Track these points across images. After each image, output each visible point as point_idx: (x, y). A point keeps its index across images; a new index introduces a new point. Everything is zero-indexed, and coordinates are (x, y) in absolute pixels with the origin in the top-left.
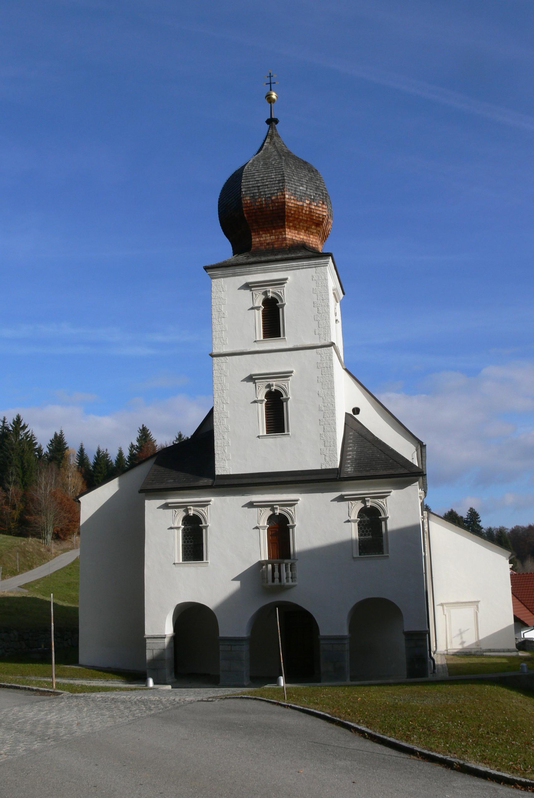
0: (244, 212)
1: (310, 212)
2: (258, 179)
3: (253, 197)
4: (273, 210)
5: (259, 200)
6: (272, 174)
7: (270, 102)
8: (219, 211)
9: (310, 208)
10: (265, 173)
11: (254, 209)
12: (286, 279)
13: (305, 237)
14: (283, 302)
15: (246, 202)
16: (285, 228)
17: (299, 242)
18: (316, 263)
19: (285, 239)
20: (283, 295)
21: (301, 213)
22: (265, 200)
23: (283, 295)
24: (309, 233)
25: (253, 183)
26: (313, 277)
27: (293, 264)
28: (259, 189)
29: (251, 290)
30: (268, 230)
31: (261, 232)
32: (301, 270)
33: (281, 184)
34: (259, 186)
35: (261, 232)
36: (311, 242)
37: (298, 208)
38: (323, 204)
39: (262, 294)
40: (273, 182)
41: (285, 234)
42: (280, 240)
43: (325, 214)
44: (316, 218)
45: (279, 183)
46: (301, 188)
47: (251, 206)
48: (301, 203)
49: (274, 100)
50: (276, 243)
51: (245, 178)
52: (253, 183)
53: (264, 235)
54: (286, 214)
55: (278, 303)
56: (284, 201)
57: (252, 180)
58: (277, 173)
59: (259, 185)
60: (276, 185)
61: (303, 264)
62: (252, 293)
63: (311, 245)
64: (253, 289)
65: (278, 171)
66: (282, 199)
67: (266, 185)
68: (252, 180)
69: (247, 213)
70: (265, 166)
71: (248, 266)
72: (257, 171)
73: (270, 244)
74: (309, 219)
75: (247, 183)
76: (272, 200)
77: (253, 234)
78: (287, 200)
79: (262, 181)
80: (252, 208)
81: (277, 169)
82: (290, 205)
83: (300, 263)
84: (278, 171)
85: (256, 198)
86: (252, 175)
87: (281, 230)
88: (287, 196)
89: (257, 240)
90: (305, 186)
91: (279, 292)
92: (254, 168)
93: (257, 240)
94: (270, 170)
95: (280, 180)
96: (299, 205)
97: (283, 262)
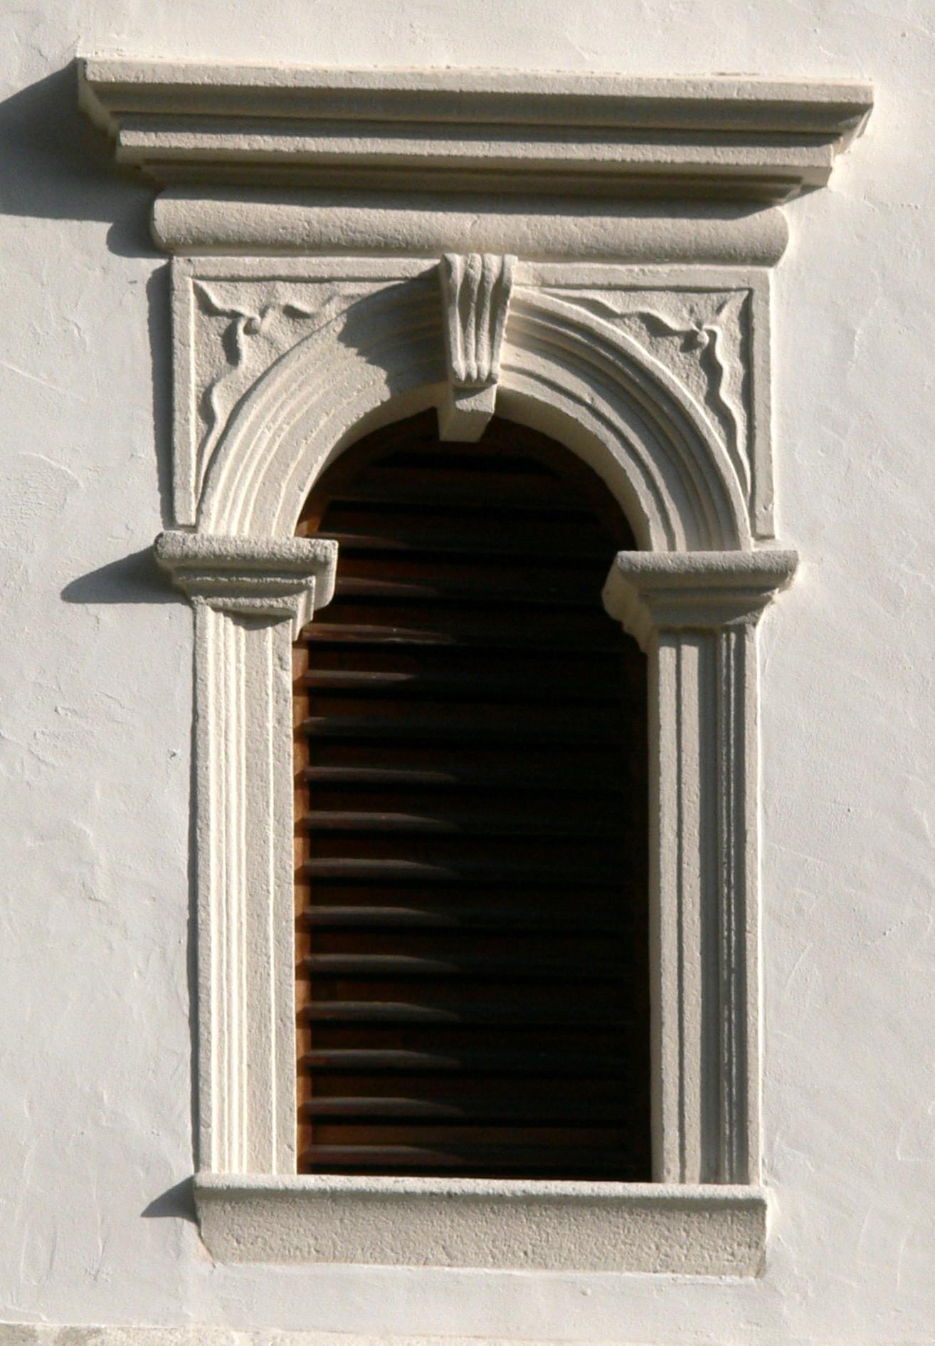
14: (731, 537)
20: (729, 396)
23: (729, 396)
39: (347, 337)
55: (634, 540)
62: (161, 289)
91: (656, 328)
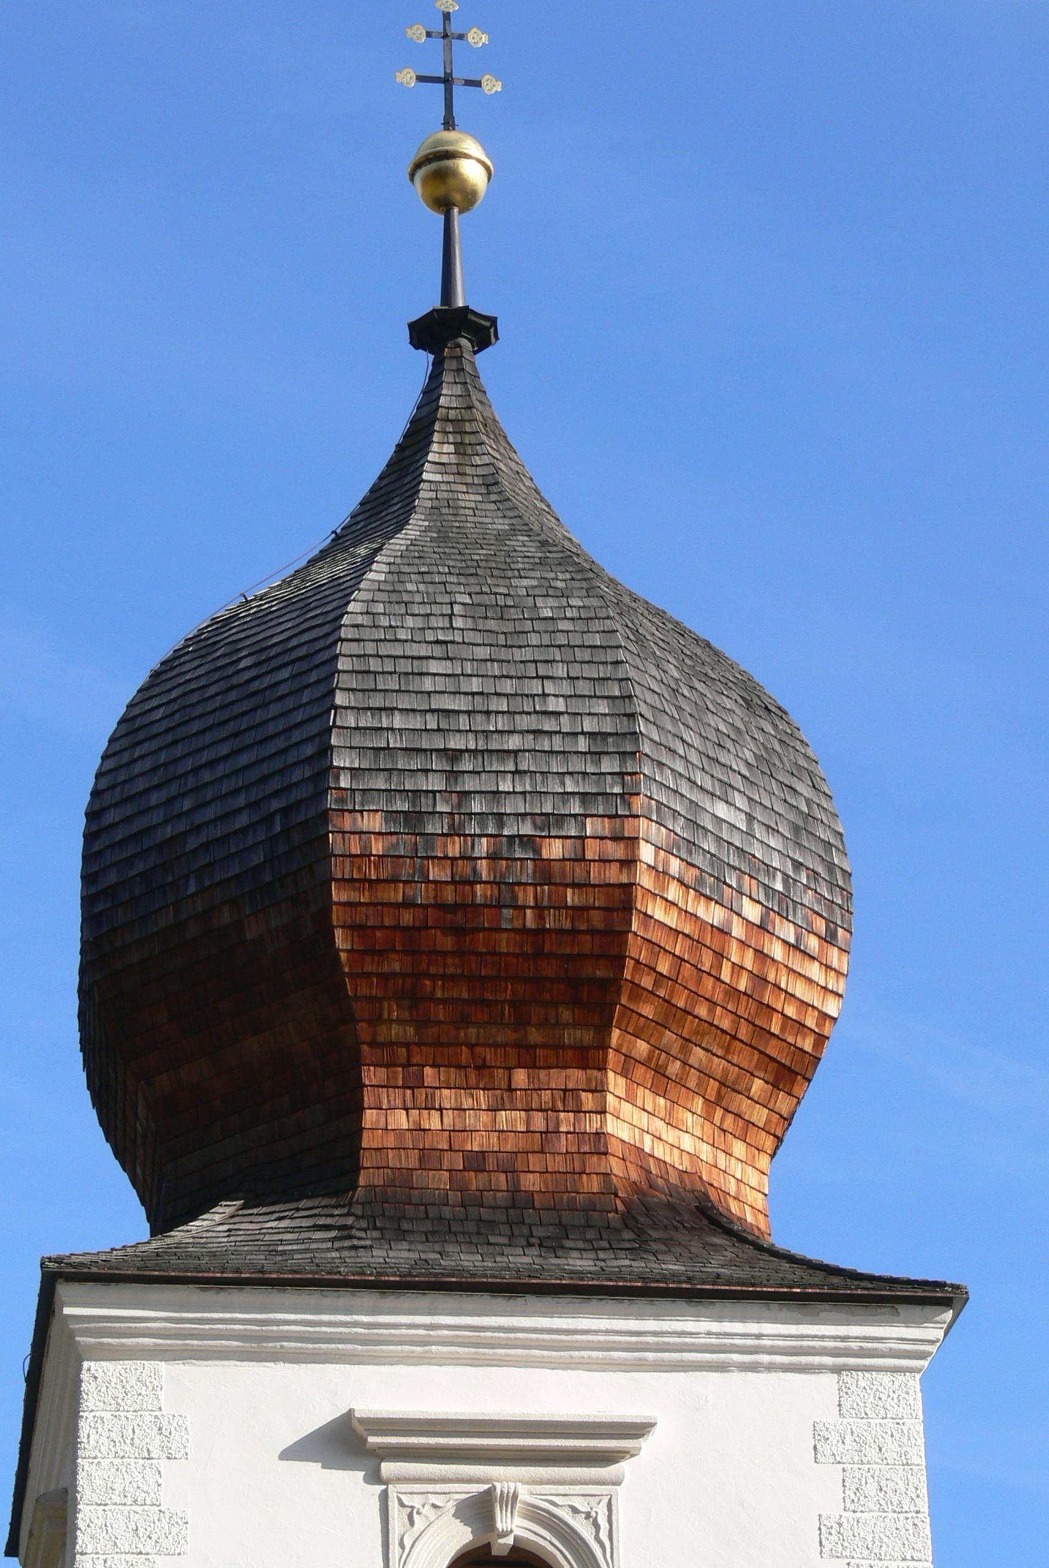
0: (336, 915)
1: (760, 980)
2: (447, 703)
3: (413, 819)
4: (541, 932)
5: (454, 848)
6: (550, 688)
7: (443, 206)
8: (88, 878)
9: (761, 956)
10: (496, 669)
11: (408, 904)
12: (638, 1430)
13: (705, 1147)
15: (356, 850)
16: (603, 1068)
17: (674, 1179)
18: (844, 1339)
19: (599, 1141)
20: (604, 1536)
21: (709, 982)
22: (493, 857)
23: (604, 1536)
24: (729, 1122)
25: (416, 722)
26: (819, 1435)
27: (689, 1325)
28: (453, 775)
29: (374, 1477)
30: (482, 1067)
31: (428, 1071)
32: (736, 1376)
33: (608, 765)
34: (455, 755)
35: (428, 1071)
36: (732, 1188)
37: (697, 943)
38: (829, 938)
40: (557, 744)
41: (603, 1112)
42: (563, 1144)
43: (832, 1007)
44: (783, 1029)
45: (596, 755)
46: (721, 810)
47: (395, 880)
48: (714, 915)
49: (469, 197)
50: (535, 1163)
51: (353, 682)
52: (416, 722)
53: (447, 1097)
54: (627, 975)
56: (624, 879)
57: (405, 702)
58: (584, 688)
59: (456, 743)
60: (577, 765)
61: (759, 1336)
62: (384, 1497)
63: (734, 1207)
64: (388, 1468)
65: (591, 672)
66: (615, 866)
67: (508, 751)
68: (405, 702)
69: (355, 928)
70: (492, 625)
71: (368, 1298)
72: (438, 651)
73: (491, 1163)
74: (744, 1032)
75: (366, 721)
76: (545, 872)
77: (371, 1075)
78: (645, 880)
79: (479, 718)
80: (397, 894)
81: (579, 654)
82: (658, 912)
83: (738, 1327)
84: (591, 672)
85: (430, 829)
86: (404, 666)
87: (576, 1077)
88: (646, 853)
89: (401, 1120)
90: (740, 801)
91: (575, 1510)
92: (410, 622)
93: (401, 1120)
94: (527, 654)
95: (605, 735)
96: (704, 923)
97: (785, 1313)
